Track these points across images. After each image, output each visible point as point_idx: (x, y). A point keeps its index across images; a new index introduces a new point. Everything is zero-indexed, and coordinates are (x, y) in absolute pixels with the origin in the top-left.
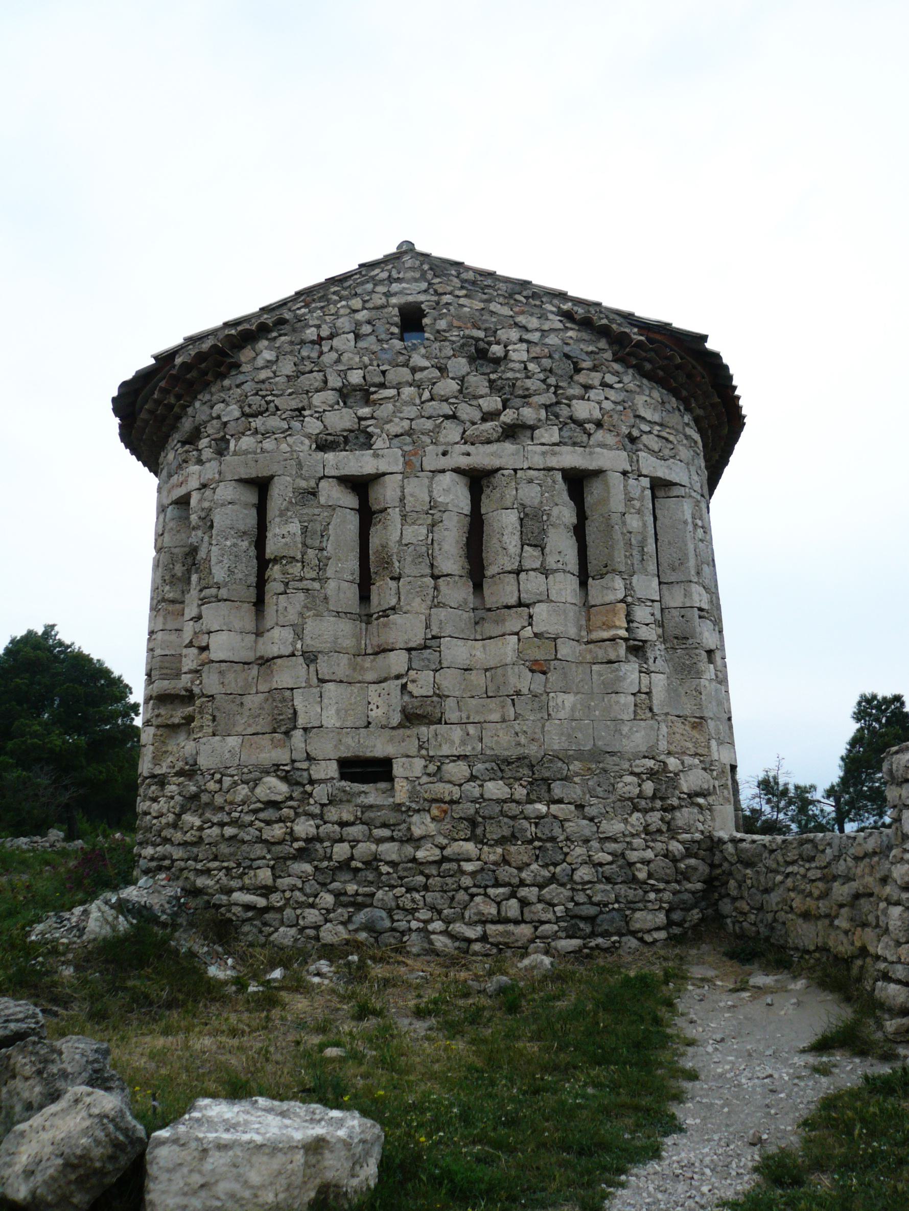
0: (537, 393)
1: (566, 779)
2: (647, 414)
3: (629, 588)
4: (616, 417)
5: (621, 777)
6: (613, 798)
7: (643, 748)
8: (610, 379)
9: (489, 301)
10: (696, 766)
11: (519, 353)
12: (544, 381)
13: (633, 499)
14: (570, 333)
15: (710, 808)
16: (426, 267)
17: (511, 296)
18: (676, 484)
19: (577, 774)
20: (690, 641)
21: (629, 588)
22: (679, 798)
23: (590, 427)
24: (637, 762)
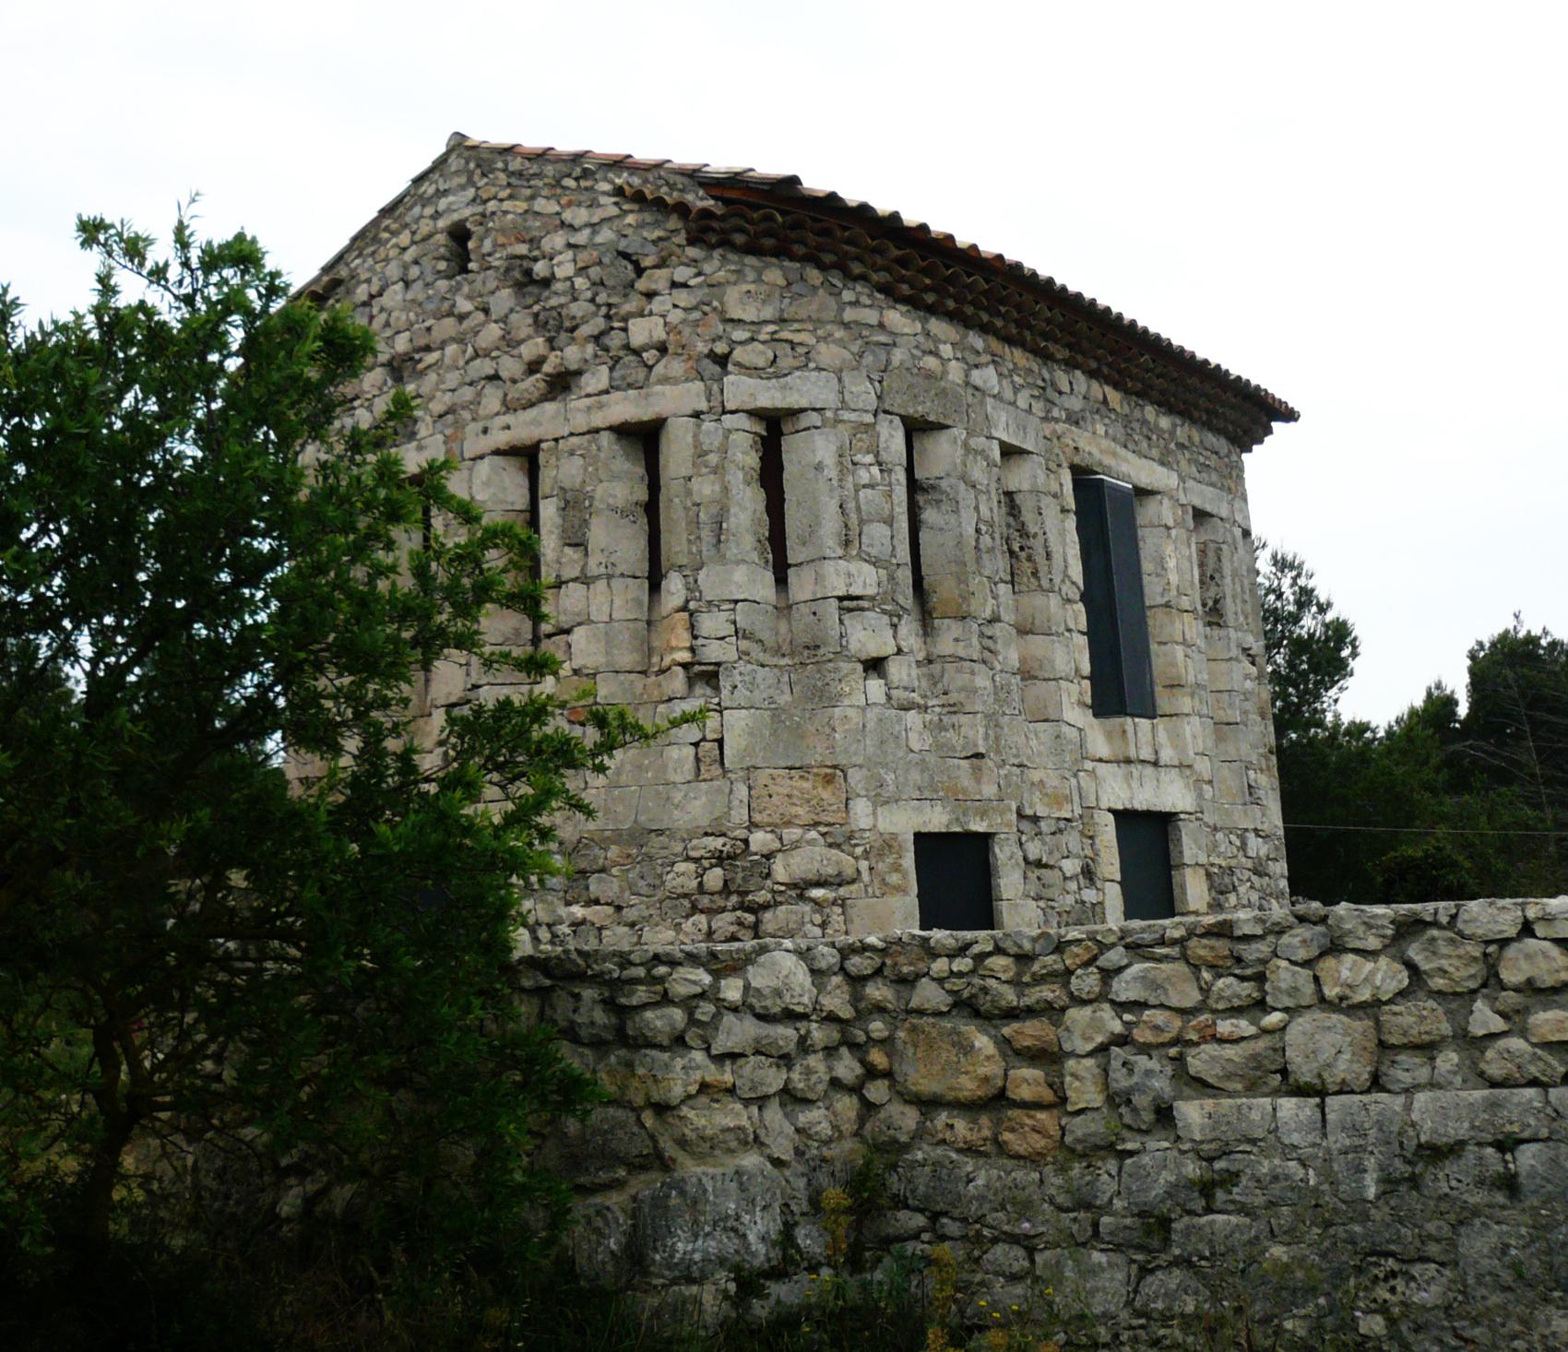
0: (585, 320)
1: (603, 870)
2: (749, 314)
3: (693, 588)
4: (687, 331)
5: (673, 864)
6: (660, 894)
7: (704, 823)
8: (681, 274)
9: (533, 198)
10: (811, 842)
11: (565, 269)
12: (592, 300)
13: (706, 453)
14: (630, 219)
15: (842, 903)
16: (472, 165)
17: (558, 183)
18: (803, 410)
19: (616, 864)
20: (821, 651)
21: (693, 588)
22: (773, 891)
23: (649, 356)
24: (695, 842)
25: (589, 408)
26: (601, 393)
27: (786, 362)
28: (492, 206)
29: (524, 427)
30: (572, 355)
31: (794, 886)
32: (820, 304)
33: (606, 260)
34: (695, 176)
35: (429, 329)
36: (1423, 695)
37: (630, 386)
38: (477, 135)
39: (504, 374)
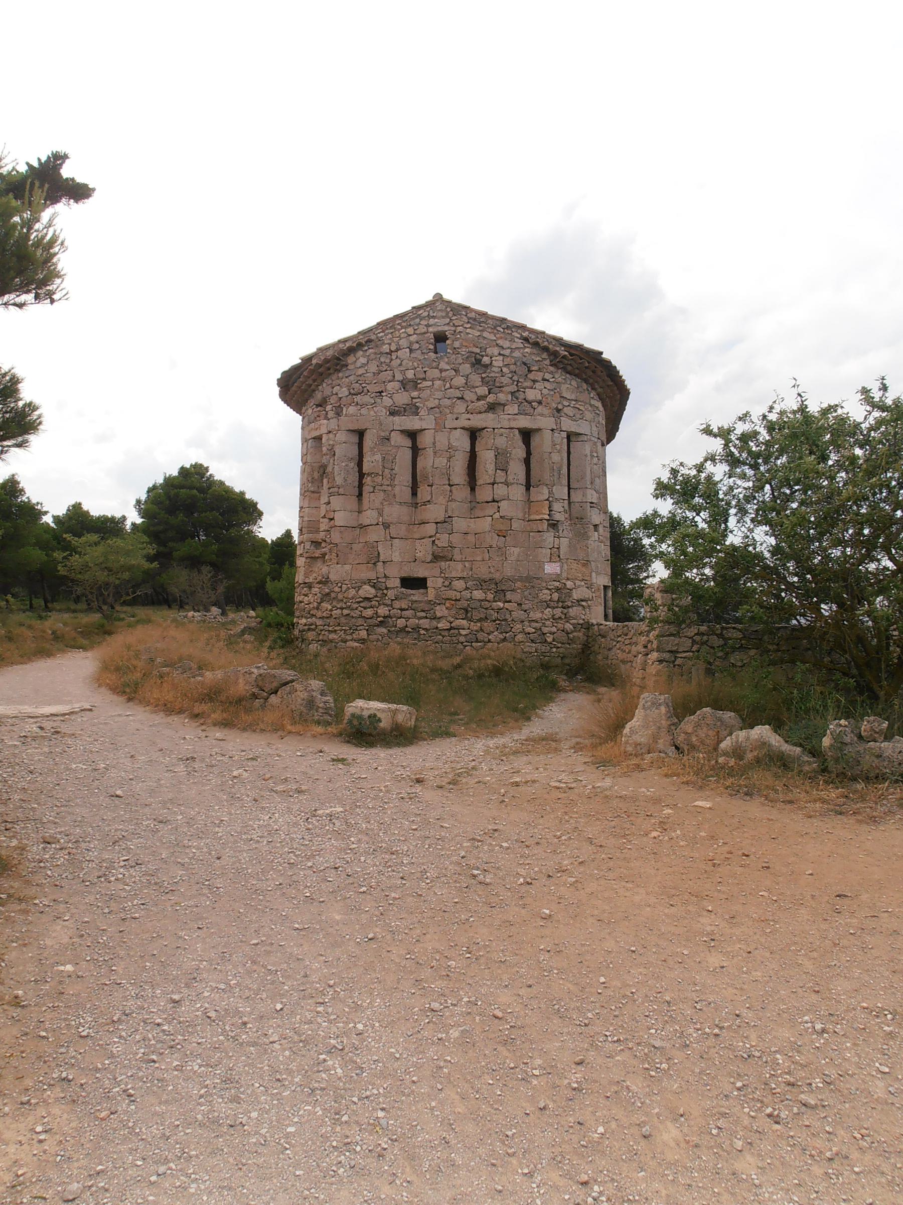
6: (536, 601)
8: (547, 376)
12: (511, 378)
14: (526, 350)
16: (449, 309)
27: (578, 416)
28: (460, 329)
29: (477, 421)
30: (502, 397)
31: (578, 601)
32: (584, 396)
33: (518, 364)
34: (559, 341)
36: (163, 478)
37: (526, 414)
38: (446, 296)
39: (467, 397)
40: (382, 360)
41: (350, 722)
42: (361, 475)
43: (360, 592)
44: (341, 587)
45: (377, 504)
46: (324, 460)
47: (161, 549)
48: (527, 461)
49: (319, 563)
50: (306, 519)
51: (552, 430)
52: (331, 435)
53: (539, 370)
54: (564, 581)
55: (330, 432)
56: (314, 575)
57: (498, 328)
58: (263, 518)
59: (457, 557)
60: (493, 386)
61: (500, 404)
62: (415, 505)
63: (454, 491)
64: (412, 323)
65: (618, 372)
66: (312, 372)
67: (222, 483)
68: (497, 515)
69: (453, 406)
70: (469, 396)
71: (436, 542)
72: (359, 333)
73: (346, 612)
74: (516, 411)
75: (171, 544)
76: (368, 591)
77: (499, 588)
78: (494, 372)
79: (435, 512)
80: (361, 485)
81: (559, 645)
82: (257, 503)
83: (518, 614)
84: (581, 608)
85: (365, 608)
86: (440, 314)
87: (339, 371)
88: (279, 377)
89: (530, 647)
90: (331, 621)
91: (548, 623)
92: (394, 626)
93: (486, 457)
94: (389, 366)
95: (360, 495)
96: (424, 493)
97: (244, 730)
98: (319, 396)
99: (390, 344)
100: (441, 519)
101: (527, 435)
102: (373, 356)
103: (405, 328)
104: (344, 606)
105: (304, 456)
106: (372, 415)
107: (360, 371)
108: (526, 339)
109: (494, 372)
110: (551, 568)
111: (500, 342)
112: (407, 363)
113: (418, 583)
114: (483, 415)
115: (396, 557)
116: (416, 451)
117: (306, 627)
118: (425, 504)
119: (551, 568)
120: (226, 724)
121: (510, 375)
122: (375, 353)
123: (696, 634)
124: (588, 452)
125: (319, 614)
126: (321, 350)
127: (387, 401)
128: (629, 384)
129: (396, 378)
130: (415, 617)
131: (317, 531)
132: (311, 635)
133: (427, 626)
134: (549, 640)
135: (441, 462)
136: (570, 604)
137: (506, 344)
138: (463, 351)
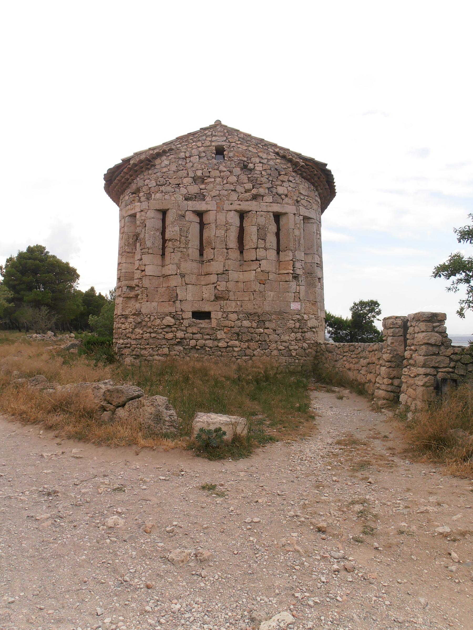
3: (294, 256)
8: (291, 179)
12: (268, 179)
14: (278, 161)
16: (225, 131)
25: (267, 206)
26: (271, 203)
27: (309, 207)
29: (245, 206)
30: (262, 191)
33: (272, 169)
34: (299, 156)
35: (209, 172)
37: (278, 203)
38: (223, 123)
40: (180, 162)
41: (199, 436)
42: (164, 241)
43: (163, 321)
44: (150, 318)
45: (176, 261)
46: (138, 230)
47: (16, 295)
48: (278, 235)
49: (133, 302)
50: (123, 271)
51: (294, 214)
52: (143, 213)
53: (286, 174)
54: (302, 315)
55: (142, 211)
56: (129, 309)
57: (259, 145)
58: (80, 278)
59: (232, 298)
60: (255, 183)
61: (260, 195)
62: (202, 262)
63: (230, 253)
64: (200, 139)
65: (333, 179)
66: (130, 169)
67: (54, 257)
68: (259, 270)
69: (229, 195)
70: (239, 189)
71: (218, 287)
72: (163, 144)
73: (153, 335)
74: (271, 201)
75: (22, 293)
76: (169, 320)
77: (260, 319)
78: (256, 174)
79: (217, 267)
80: (164, 248)
81: (300, 358)
82: (76, 270)
83: (274, 337)
84: (312, 333)
85: (167, 333)
86: (220, 134)
87: (149, 169)
88: (106, 172)
89: (283, 359)
90: (142, 341)
91: (293, 343)
92: (187, 345)
93: (251, 231)
94: (185, 167)
95: (163, 255)
96: (208, 253)
97: (99, 444)
98: (134, 187)
99: (185, 152)
100: (220, 271)
101: (277, 217)
102: (173, 160)
103: (196, 142)
104: (152, 331)
105: (122, 228)
106: (174, 200)
107: (165, 170)
108: (277, 154)
109: (256, 174)
110: (295, 306)
111: (260, 154)
112: (197, 166)
113: (206, 315)
114: (249, 203)
115: (190, 297)
116: (202, 225)
117: (123, 346)
118: (209, 261)
119: (295, 306)
120: (80, 437)
121: (267, 177)
122: (175, 158)
123: (452, 354)
124: (315, 230)
125: (133, 336)
126: (136, 154)
127: (183, 191)
128: (337, 189)
129: (190, 176)
130: (203, 338)
131: (132, 279)
132: (126, 351)
133: (211, 345)
134: (294, 354)
135: (221, 233)
136: (306, 330)
137: (265, 156)
138: (236, 159)
